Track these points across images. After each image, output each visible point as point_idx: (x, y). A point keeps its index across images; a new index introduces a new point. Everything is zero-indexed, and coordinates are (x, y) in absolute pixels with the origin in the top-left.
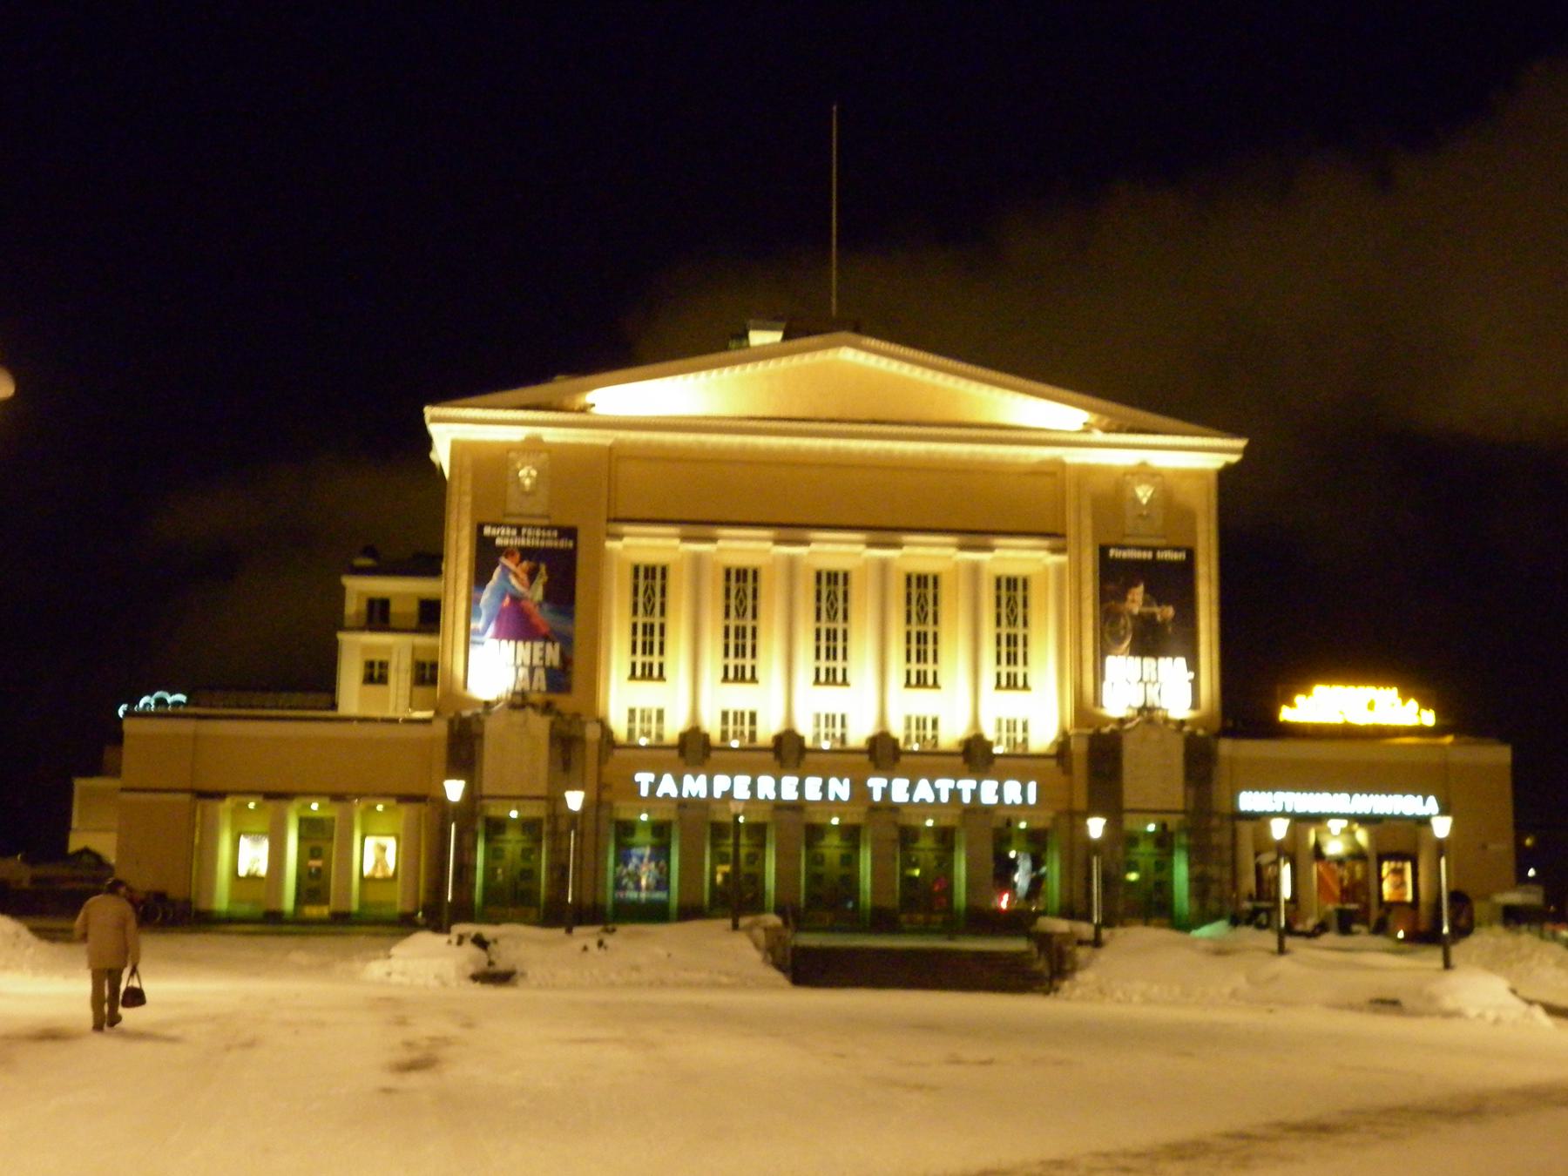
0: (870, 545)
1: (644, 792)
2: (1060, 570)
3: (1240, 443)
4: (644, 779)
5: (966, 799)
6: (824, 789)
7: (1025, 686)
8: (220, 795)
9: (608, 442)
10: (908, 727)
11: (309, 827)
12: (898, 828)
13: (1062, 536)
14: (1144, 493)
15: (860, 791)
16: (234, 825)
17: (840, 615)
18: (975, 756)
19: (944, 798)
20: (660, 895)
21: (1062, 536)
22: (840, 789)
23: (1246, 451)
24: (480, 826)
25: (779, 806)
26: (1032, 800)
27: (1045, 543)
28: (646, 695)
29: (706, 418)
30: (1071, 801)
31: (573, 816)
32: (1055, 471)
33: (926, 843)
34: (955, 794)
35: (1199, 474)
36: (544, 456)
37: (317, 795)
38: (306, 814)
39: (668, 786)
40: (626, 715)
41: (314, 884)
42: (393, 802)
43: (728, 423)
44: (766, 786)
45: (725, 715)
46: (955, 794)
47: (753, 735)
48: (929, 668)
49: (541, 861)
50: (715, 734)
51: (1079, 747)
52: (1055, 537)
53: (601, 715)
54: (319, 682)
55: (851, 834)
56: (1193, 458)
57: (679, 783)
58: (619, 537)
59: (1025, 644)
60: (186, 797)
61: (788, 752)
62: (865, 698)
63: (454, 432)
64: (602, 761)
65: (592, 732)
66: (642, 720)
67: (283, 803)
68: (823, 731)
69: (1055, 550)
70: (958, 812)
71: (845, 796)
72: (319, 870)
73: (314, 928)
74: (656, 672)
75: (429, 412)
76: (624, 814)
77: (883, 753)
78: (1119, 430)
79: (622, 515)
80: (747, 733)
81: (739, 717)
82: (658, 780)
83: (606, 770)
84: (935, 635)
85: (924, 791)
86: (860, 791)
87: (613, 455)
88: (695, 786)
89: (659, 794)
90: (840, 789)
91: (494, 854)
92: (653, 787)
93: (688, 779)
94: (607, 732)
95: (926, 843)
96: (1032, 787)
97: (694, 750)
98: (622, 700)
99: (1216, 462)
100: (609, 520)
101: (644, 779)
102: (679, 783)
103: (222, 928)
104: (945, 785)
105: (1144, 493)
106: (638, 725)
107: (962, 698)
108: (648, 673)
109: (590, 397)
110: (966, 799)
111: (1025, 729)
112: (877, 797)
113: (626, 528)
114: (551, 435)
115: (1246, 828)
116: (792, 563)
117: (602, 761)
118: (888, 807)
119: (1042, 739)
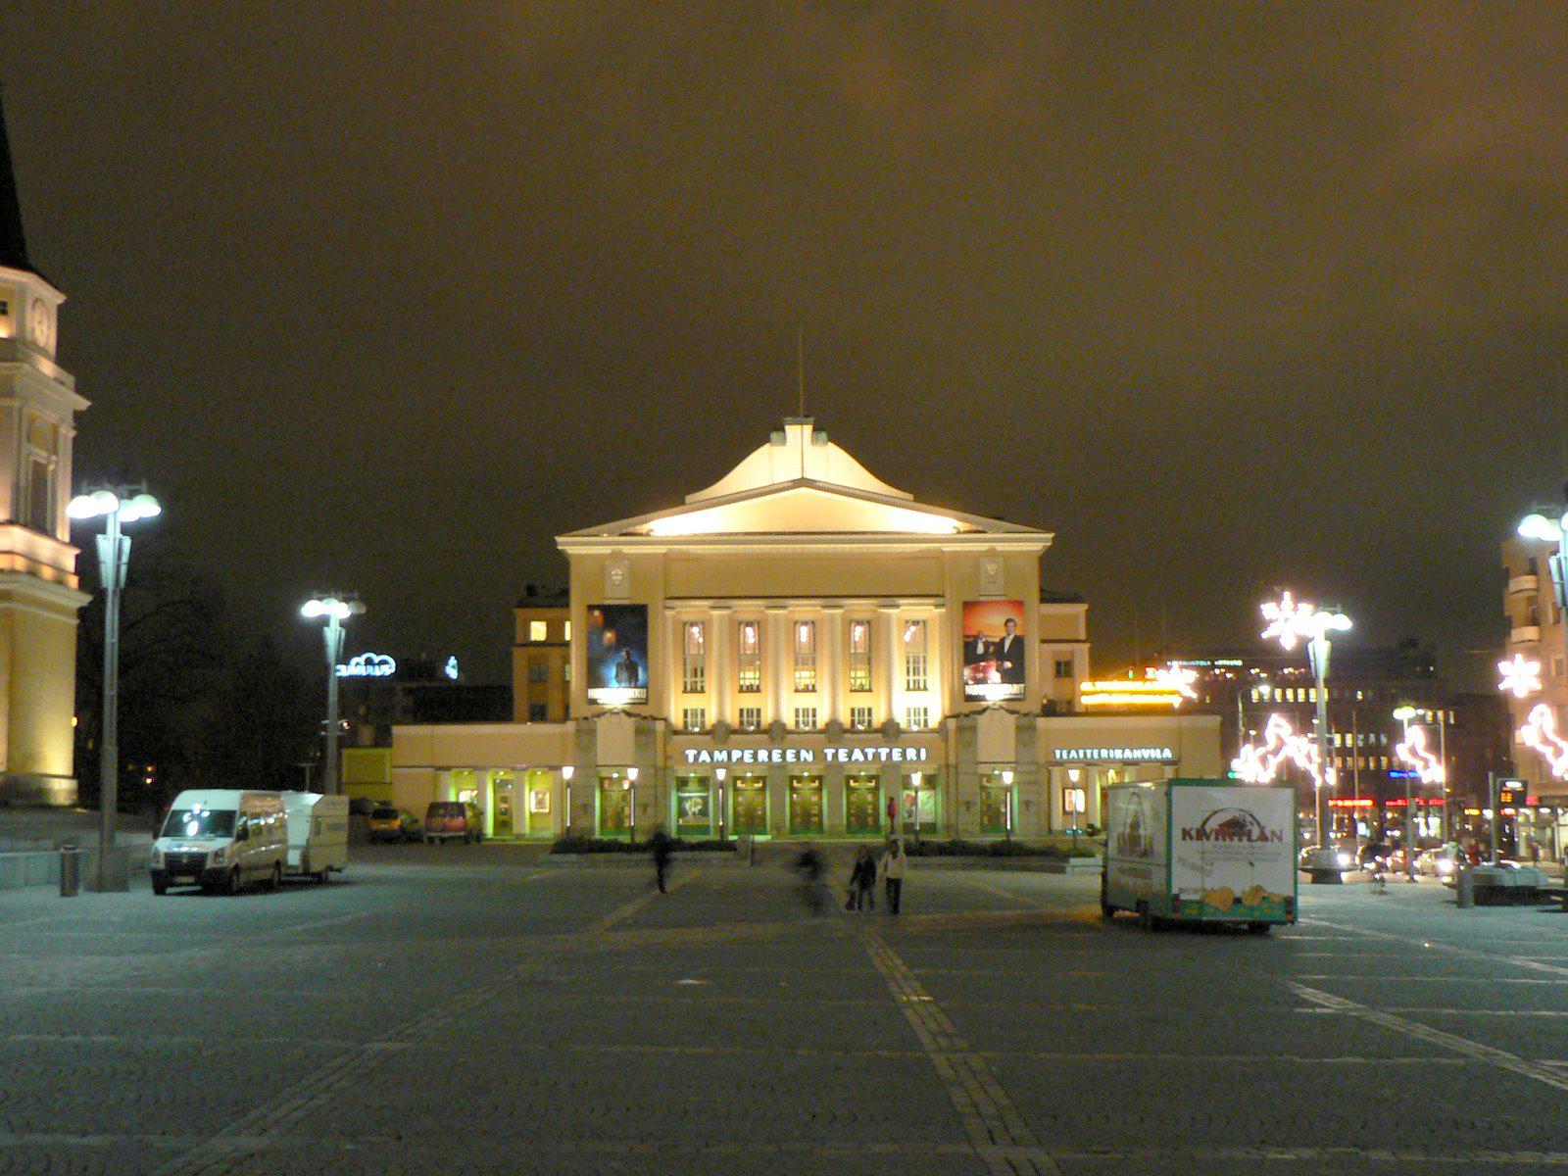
0: (824, 607)
3: (1051, 535)
4: (691, 753)
5: (883, 758)
6: (798, 755)
7: (925, 689)
8: (448, 769)
9: (665, 551)
10: (797, 716)
11: (499, 786)
15: (819, 756)
16: (456, 787)
19: (870, 757)
20: (702, 822)
21: (943, 596)
27: (931, 601)
28: (693, 702)
29: (694, 535)
30: (947, 757)
34: (877, 755)
35: (1030, 552)
37: (503, 767)
40: (849, 712)
41: (504, 818)
42: (546, 769)
43: (712, 538)
45: (853, 711)
46: (877, 755)
48: (921, 678)
50: (903, 726)
54: (1315, 703)
59: (925, 662)
63: (576, 546)
64: (665, 743)
66: (692, 715)
67: (482, 773)
68: (912, 718)
72: (506, 809)
73: (1035, 861)
75: (559, 539)
76: (682, 774)
77: (835, 732)
80: (811, 722)
82: (699, 753)
83: (669, 748)
84: (924, 658)
89: (700, 760)
92: (696, 758)
97: (721, 734)
99: (1038, 547)
103: (1013, 861)
104: (870, 752)
106: (801, 719)
108: (916, 687)
110: (883, 758)
111: (870, 714)
112: (830, 758)
114: (1000, 547)
115: (1056, 771)
116: (832, 618)
117: (665, 743)
118: (836, 764)
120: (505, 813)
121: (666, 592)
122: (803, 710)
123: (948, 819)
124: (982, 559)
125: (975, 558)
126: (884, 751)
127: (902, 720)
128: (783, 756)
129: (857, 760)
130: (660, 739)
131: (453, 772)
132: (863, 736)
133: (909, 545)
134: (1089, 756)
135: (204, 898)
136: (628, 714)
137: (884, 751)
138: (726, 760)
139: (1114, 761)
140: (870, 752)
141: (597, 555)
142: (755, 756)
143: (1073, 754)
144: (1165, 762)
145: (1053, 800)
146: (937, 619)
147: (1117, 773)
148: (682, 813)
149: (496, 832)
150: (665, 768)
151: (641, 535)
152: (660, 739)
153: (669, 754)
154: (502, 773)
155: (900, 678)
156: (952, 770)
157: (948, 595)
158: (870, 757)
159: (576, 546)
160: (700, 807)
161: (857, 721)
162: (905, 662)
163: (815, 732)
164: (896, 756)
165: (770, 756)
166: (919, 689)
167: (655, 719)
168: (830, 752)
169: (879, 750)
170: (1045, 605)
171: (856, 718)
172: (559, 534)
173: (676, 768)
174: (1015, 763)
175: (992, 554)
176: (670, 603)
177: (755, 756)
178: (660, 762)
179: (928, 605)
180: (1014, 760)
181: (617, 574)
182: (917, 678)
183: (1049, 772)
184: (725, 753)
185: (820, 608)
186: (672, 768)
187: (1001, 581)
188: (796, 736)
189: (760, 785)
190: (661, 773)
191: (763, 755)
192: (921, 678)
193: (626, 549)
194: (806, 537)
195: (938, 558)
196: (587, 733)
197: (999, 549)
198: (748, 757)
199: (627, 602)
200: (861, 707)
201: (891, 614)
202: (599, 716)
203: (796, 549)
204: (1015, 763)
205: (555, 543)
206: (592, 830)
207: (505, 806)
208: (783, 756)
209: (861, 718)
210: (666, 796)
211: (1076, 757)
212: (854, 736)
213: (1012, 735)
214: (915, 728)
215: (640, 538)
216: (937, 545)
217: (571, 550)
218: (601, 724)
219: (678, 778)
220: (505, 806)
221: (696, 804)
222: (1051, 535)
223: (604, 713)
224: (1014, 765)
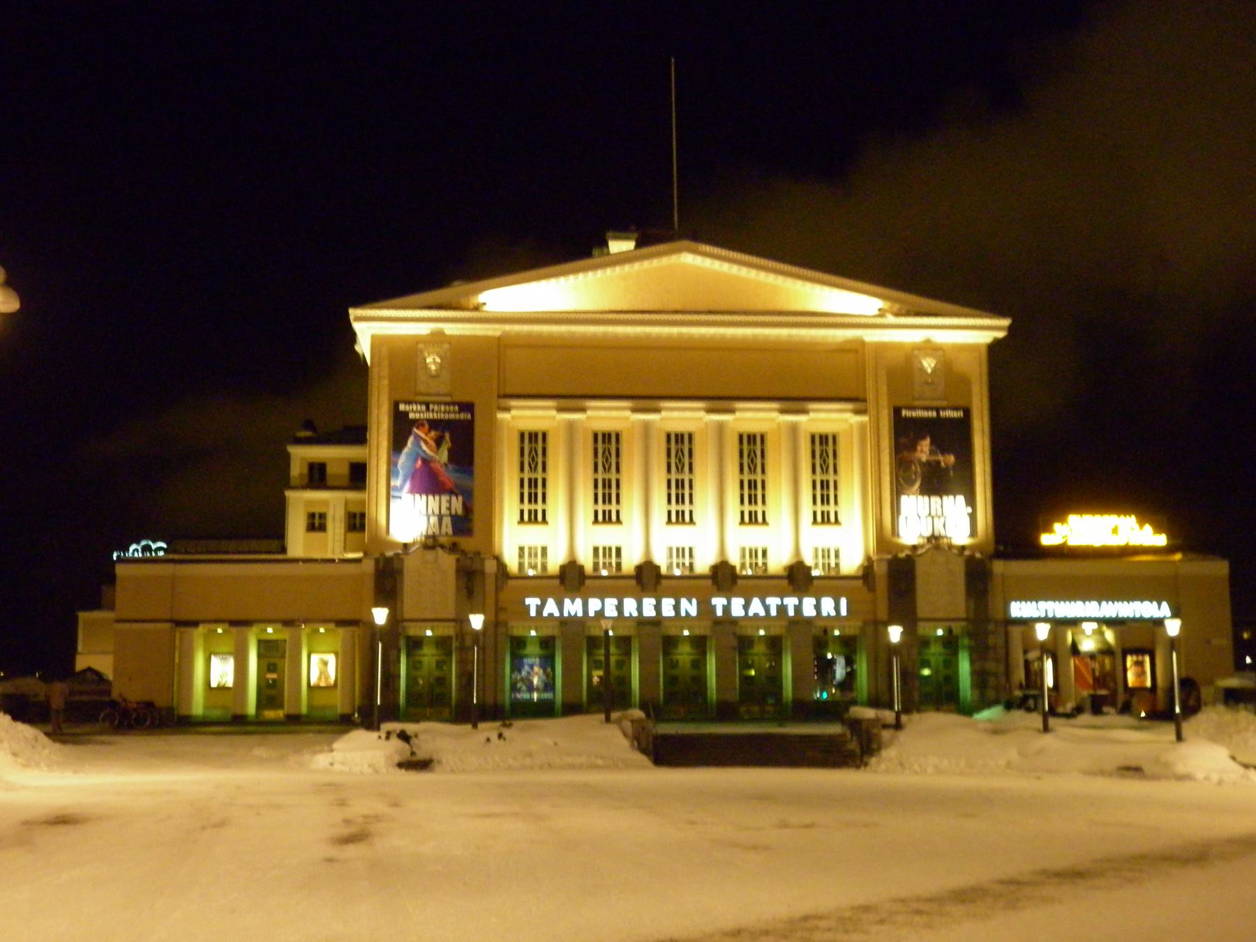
1: (533, 613)
2: (862, 427)
3: (1006, 322)
4: (532, 602)
6: (677, 607)
8: (195, 624)
9: (498, 334)
11: (267, 648)
12: (736, 638)
13: (865, 400)
14: (929, 364)
15: (706, 608)
17: (686, 468)
18: (797, 578)
19: (773, 613)
22: (690, 607)
23: (1010, 329)
24: (402, 643)
25: (641, 622)
26: (844, 612)
27: (849, 406)
28: (533, 536)
31: (476, 634)
32: (857, 348)
33: (760, 649)
34: (782, 609)
37: (270, 621)
38: (264, 637)
39: (551, 608)
40: (517, 552)
41: (273, 692)
42: (332, 626)
44: (630, 606)
45: (596, 550)
46: (782, 609)
47: (619, 565)
49: (452, 670)
51: (881, 570)
52: (857, 400)
53: (497, 552)
55: (699, 643)
56: (968, 334)
57: (560, 605)
58: (507, 409)
60: (167, 626)
61: (647, 578)
62: (709, 534)
63: (374, 328)
64: (498, 589)
65: (490, 567)
66: (530, 555)
67: (243, 629)
68: (675, 561)
69: (857, 412)
70: (784, 623)
71: (694, 612)
72: (274, 680)
74: (540, 517)
75: (353, 312)
77: (723, 577)
79: (509, 390)
81: (607, 551)
83: (503, 596)
84: (691, 481)
85: (756, 607)
86: (706, 608)
87: (501, 344)
88: (573, 607)
89: (545, 614)
90: (690, 607)
91: (414, 666)
92: (540, 609)
93: (567, 601)
94: (501, 566)
95: (760, 649)
96: (843, 601)
97: (572, 578)
98: (514, 540)
99: (986, 337)
100: (499, 397)
101: (532, 602)
102: (560, 605)
104: (773, 602)
105: (929, 364)
106: (601, 560)
107: (784, 534)
109: (483, 297)
110: (791, 613)
112: (719, 613)
113: (514, 403)
114: (451, 329)
115: (1016, 632)
116: (646, 427)
117: (498, 589)
118: (728, 620)
119: (851, 563)
120: (275, 685)
122: (604, 549)
123: (876, 688)
127: (661, 560)
128: (658, 607)
129: (756, 615)
131: (202, 629)
132: (607, 582)
137: (791, 602)
138: (580, 614)
149: (260, 705)
154: (270, 630)
155: (585, 507)
161: (526, 565)
162: (738, 486)
163: (544, 577)
164: (611, 611)
166: (610, 520)
168: (719, 602)
171: (526, 560)
173: (511, 623)
175: (437, 339)
179: (698, 409)
180: (452, 616)
182: (753, 508)
183: (1007, 634)
184: (579, 601)
185: (554, 413)
186: (505, 624)
188: (520, 582)
192: (613, 507)
194: (647, 317)
195: (856, 351)
198: (611, 611)
200: (607, 545)
201: (727, 422)
207: (274, 676)
208: (658, 607)
209: (607, 560)
212: (597, 582)
214: (677, 572)
219: (408, 638)
220: (274, 676)
222: (1006, 322)
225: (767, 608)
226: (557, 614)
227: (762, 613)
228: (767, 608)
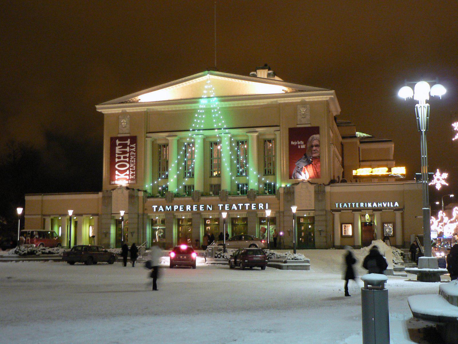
19: (240, 208)
21: (279, 126)
34: (244, 207)
36: (128, 117)
44: (362, 205)
46: (244, 207)
63: (107, 109)
75: (97, 106)
78: (296, 92)
83: (146, 205)
92: (157, 209)
104: (240, 205)
109: (139, 97)
114: (307, 99)
117: (144, 202)
121: (147, 130)
124: (298, 106)
125: (294, 106)
126: (247, 205)
130: (141, 200)
133: (261, 101)
134: (389, 206)
135: (409, 282)
136: (311, 183)
137: (247, 205)
139: (368, 209)
140: (240, 205)
141: (292, 103)
142: (184, 208)
143: (375, 204)
144: (396, 209)
145: (335, 232)
146: (255, 136)
147: (370, 215)
148: (153, 236)
150: (143, 214)
151: (133, 102)
152: (141, 200)
153: (145, 207)
156: (141, 217)
157: (281, 124)
158: (240, 208)
159: (107, 109)
160: (162, 234)
165: (192, 208)
167: (139, 190)
169: (245, 204)
170: (317, 126)
172: (97, 104)
174: (314, 210)
175: (303, 104)
176: (148, 135)
177: (184, 208)
178: (141, 211)
180: (314, 209)
181: (124, 122)
187: (308, 117)
189: (190, 223)
190: (141, 217)
191: (188, 208)
193: (128, 110)
196: (108, 199)
197: (307, 100)
199: (309, 126)
202: (113, 190)
203: (150, 109)
204: (314, 210)
205: (95, 108)
206: (108, 246)
210: (144, 229)
211: (376, 206)
213: (127, 200)
215: (132, 104)
216: (275, 100)
217: (105, 111)
218: (114, 193)
221: (160, 232)
223: (298, 183)
224: (314, 211)
225: (238, 207)
226: (376, 206)
227: (236, 209)
228: (238, 207)
